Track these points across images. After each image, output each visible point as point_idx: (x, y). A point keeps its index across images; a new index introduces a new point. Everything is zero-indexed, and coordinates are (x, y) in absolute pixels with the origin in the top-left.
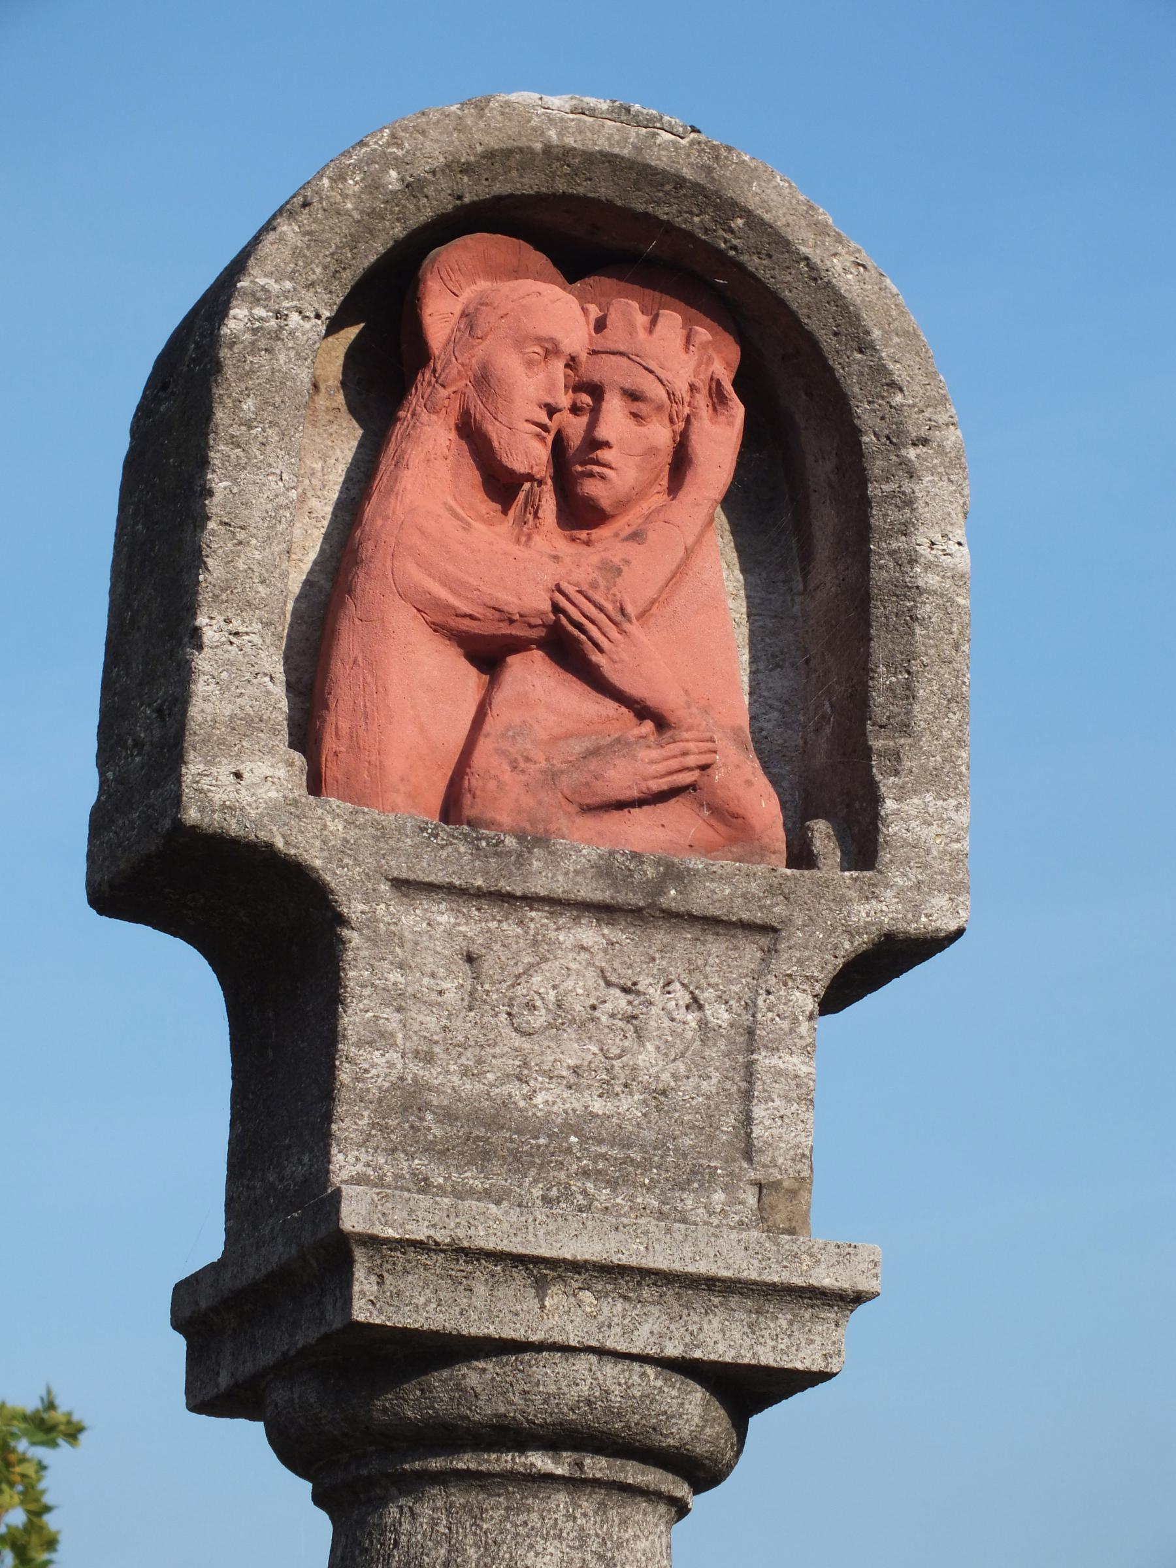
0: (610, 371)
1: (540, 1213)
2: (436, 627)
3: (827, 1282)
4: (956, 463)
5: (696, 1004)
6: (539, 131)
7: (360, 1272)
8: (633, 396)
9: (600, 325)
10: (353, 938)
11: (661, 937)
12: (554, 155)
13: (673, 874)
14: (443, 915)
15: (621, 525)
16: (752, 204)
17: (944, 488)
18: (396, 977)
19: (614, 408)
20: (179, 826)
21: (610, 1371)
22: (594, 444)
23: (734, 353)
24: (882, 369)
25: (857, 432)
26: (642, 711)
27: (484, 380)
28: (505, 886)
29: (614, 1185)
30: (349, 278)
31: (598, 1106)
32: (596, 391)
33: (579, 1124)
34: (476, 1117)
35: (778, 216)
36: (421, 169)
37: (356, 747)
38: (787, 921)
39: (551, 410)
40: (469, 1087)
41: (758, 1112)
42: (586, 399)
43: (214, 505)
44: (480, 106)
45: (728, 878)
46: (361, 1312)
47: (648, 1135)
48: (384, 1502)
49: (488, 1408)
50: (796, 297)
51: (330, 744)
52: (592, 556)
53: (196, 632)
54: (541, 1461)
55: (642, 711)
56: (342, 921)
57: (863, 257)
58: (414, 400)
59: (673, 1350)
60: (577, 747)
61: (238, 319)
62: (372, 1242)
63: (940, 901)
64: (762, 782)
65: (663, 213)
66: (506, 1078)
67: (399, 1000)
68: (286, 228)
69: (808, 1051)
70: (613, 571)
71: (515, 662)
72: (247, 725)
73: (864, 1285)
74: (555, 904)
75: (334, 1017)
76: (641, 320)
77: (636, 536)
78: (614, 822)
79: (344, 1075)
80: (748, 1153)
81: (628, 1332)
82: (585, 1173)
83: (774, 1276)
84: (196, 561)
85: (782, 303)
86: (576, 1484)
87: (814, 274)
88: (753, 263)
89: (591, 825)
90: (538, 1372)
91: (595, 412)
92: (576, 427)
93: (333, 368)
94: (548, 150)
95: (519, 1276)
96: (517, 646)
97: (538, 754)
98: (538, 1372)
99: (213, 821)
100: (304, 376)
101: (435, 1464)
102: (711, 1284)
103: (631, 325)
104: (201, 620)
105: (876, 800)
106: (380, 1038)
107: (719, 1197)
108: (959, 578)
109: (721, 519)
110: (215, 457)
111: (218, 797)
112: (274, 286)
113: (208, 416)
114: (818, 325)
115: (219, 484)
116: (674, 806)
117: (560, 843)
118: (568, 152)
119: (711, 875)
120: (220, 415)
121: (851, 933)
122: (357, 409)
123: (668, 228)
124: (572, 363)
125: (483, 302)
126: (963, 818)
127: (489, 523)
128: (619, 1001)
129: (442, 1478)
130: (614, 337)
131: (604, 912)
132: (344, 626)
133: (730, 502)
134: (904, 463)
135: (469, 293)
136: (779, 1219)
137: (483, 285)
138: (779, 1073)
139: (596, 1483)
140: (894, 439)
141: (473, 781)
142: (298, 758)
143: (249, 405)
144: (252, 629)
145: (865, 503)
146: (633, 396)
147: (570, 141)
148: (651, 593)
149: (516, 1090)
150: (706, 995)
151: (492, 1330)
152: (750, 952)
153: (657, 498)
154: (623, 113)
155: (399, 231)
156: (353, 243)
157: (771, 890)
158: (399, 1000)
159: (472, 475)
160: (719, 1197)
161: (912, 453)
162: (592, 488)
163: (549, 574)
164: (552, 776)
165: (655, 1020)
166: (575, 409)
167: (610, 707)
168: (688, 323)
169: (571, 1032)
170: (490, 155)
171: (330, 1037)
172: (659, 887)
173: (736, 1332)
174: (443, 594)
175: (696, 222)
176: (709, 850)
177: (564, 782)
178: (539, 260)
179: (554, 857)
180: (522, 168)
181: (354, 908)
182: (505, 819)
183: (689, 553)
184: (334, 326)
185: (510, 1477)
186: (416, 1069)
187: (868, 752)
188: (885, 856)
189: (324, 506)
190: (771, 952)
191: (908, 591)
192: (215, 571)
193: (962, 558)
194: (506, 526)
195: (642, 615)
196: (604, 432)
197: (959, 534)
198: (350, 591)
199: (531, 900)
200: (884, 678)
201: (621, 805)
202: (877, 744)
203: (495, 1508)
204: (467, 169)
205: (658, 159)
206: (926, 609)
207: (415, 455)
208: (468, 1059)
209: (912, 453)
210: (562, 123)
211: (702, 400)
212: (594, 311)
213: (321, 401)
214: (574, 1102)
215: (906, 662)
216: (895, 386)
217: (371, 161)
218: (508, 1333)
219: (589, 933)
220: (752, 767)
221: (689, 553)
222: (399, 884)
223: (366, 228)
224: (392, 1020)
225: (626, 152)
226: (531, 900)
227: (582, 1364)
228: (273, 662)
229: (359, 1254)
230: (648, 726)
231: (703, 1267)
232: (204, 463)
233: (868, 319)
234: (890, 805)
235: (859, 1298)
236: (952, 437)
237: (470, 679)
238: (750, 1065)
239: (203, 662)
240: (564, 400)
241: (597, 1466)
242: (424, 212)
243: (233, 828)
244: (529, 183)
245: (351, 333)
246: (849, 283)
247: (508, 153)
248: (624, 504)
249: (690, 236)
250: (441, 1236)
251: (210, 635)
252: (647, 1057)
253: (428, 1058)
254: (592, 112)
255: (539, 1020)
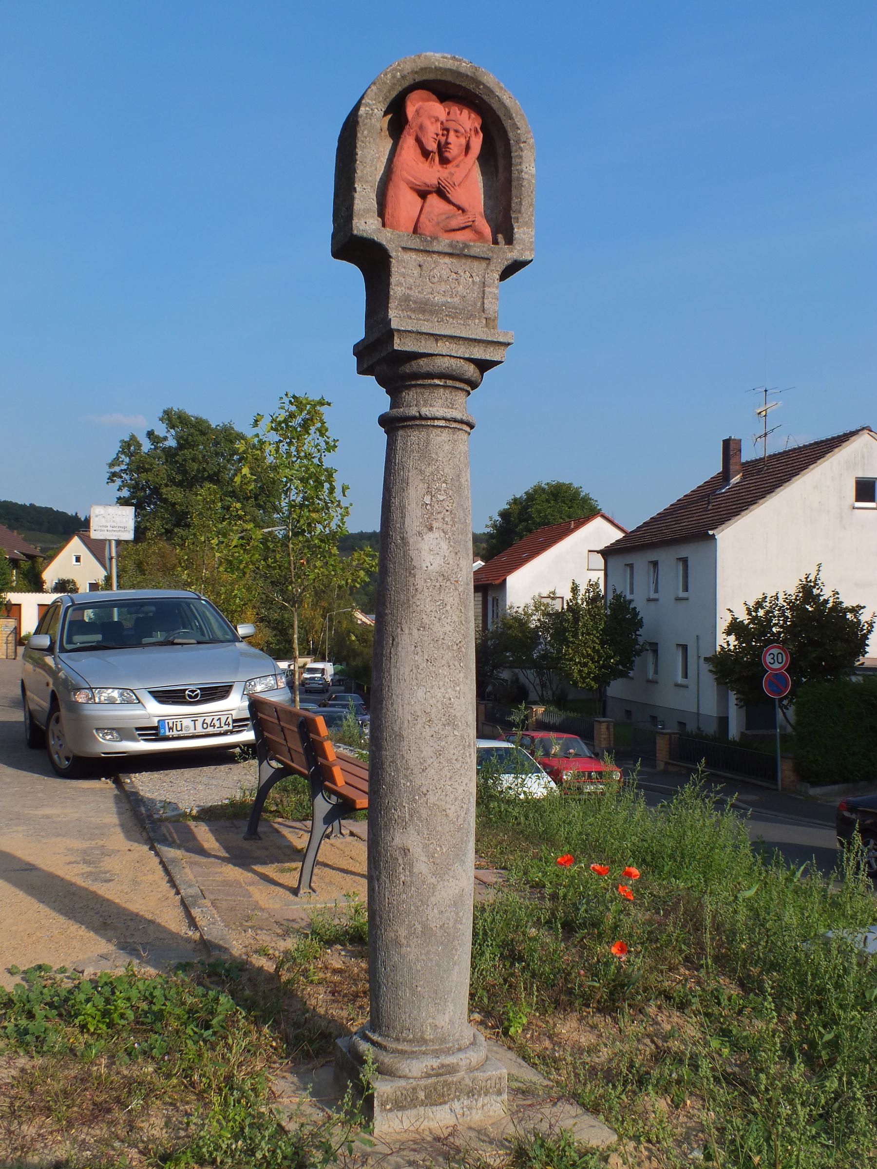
0: (451, 125)
1: (437, 324)
2: (411, 188)
3: (501, 340)
4: (532, 147)
5: (471, 276)
6: (434, 63)
7: (395, 338)
8: (456, 131)
9: (449, 113)
10: (393, 261)
11: (463, 261)
12: (437, 69)
13: (466, 246)
14: (414, 256)
15: (454, 163)
16: (485, 82)
17: (529, 154)
18: (403, 270)
19: (452, 134)
20: (352, 235)
21: (453, 360)
22: (447, 143)
23: (480, 121)
24: (515, 124)
25: (509, 140)
26: (459, 208)
27: (421, 127)
28: (428, 249)
29: (453, 318)
30: (389, 100)
31: (449, 300)
32: (448, 130)
33: (444, 304)
34: (421, 302)
35: (491, 85)
36: (405, 73)
37: (393, 216)
38: (492, 257)
39: (437, 135)
40: (420, 296)
41: (486, 301)
42: (445, 132)
43: (358, 157)
44: (419, 56)
45: (479, 247)
46: (396, 347)
47: (461, 307)
48: (402, 392)
49: (424, 370)
50: (495, 106)
51: (387, 216)
52: (447, 171)
53: (355, 188)
54: (437, 382)
55: (459, 208)
56: (390, 257)
57: (511, 95)
58: (405, 133)
59: (467, 356)
60: (444, 217)
61: (362, 111)
62: (398, 331)
63: (528, 253)
64: (487, 225)
65: (464, 84)
66: (429, 293)
67: (404, 275)
68: (373, 87)
69: (497, 287)
70: (452, 174)
71: (430, 197)
72: (367, 211)
73: (510, 341)
74: (440, 253)
75: (389, 279)
76: (458, 112)
77: (457, 166)
78: (452, 234)
79: (392, 293)
80: (483, 311)
81: (456, 352)
82: (446, 315)
83: (490, 339)
84: (354, 171)
85: (491, 108)
86: (445, 387)
87: (500, 100)
88: (485, 97)
89: (446, 235)
90: (436, 361)
91: (447, 136)
92: (443, 139)
93: (385, 126)
94: (436, 68)
95: (432, 338)
96: (430, 192)
97: (435, 219)
98: (436, 361)
99: (360, 234)
100: (378, 125)
101: (413, 383)
102: (475, 340)
103: (456, 113)
104: (356, 186)
105: (513, 229)
106: (400, 284)
107: (477, 321)
108: (532, 176)
109: (477, 163)
110: (358, 145)
111: (361, 228)
112: (371, 102)
113: (356, 135)
114: (501, 113)
115: (359, 152)
116: (467, 231)
117: (440, 239)
118: (441, 68)
119: (475, 246)
120: (359, 135)
121: (507, 260)
122: (391, 136)
123: (465, 88)
124: (442, 123)
125: (421, 108)
126: (533, 233)
127: (423, 163)
128: (455, 276)
129: (415, 386)
130: (452, 117)
131: (451, 255)
132: (390, 188)
133: (478, 159)
134: (520, 148)
135: (417, 105)
136: (491, 326)
137: (421, 103)
138: (490, 293)
139: (450, 386)
140: (518, 142)
141: (420, 225)
142: (380, 219)
143: (366, 132)
144: (368, 188)
145: (511, 158)
146: (456, 131)
147: (441, 65)
148: (461, 179)
149: (431, 296)
150: (474, 275)
151: (425, 351)
152: (484, 264)
153: (462, 157)
154: (454, 58)
155: (400, 89)
156: (389, 91)
157: (488, 250)
158: (404, 275)
159: (419, 151)
160: (477, 321)
161: (522, 145)
162: (447, 154)
163: (437, 175)
164: (438, 224)
165: (462, 280)
166: (443, 135)
167: (452, 207)
168: (469, 113)
169: (443, 283)
170: (422, 69)
171: (388, 284)
172: (463, 249)
173: (481, 351)
174: (413, 180)
175: (471, 87)
176: (474, 241)
177: (441, 225)
178: (434, 97)
179: (439, 242)
180: (430, 72)
181: (393, 254)
182: (427, 233)
183: (469, 170)
184: (386, 114)
185: (430, 385)
186: (408, 291)
187: (511, 218)
188: (515, 242)
189: (384, 160)
190: (488, 264)
191: (520, 179)
192: (359, 173)
193: (533, 171)
194: (427, 164)
195: (459, 185)
196: (450, 140)
197: (533, 165)
198: (391, 179)
199: (434, 252)
200: (515, 200)
201: (454, 230)
202: (513, 216)
203: (427, 392)
204: (416, 72)
205: (462, 70)
206: (525, 183)
207: (405, 146)
208: (420, 289)
209: (522, 145)
210: (439, 62)
211: (473, 132)
212: (447, 110)
213: (383, 134)
214: (444, 299)
215: (520, 196)
216: (518, 128)
217: (393, 70)
218: (430, 352)
219: (447, 260)
220: (484, 221)
221: (469, 170)
222: (403, 248)
223: (392, 88)
224: (402, 280)
225: (454, 68)
226: (434, 252)
227: (446, 359)
228: (373, 196)
229: (395, 334)
230: (460, 212)
231: (473, 337)
232: (355, 147)
233: (512, 111)
234: (516, 230)
235: (509, 344)
236: (532, 141)
237: (419, 201)
238: (484, 291)
239: (356, 195)
240: (440, 132)
241: (450, 383)
242: (406, 84)
243: (365, 235)
244: (431, 76)
245: (390, 116)
246: (507, 102)
247: (426, 68)
248: (454, 158)
249: (470, 90)
250: (414, 329)
251: (358, 189)
252: (460, 288)
253: (411, 289)
254: (446, 58)
255: (436, 280)
